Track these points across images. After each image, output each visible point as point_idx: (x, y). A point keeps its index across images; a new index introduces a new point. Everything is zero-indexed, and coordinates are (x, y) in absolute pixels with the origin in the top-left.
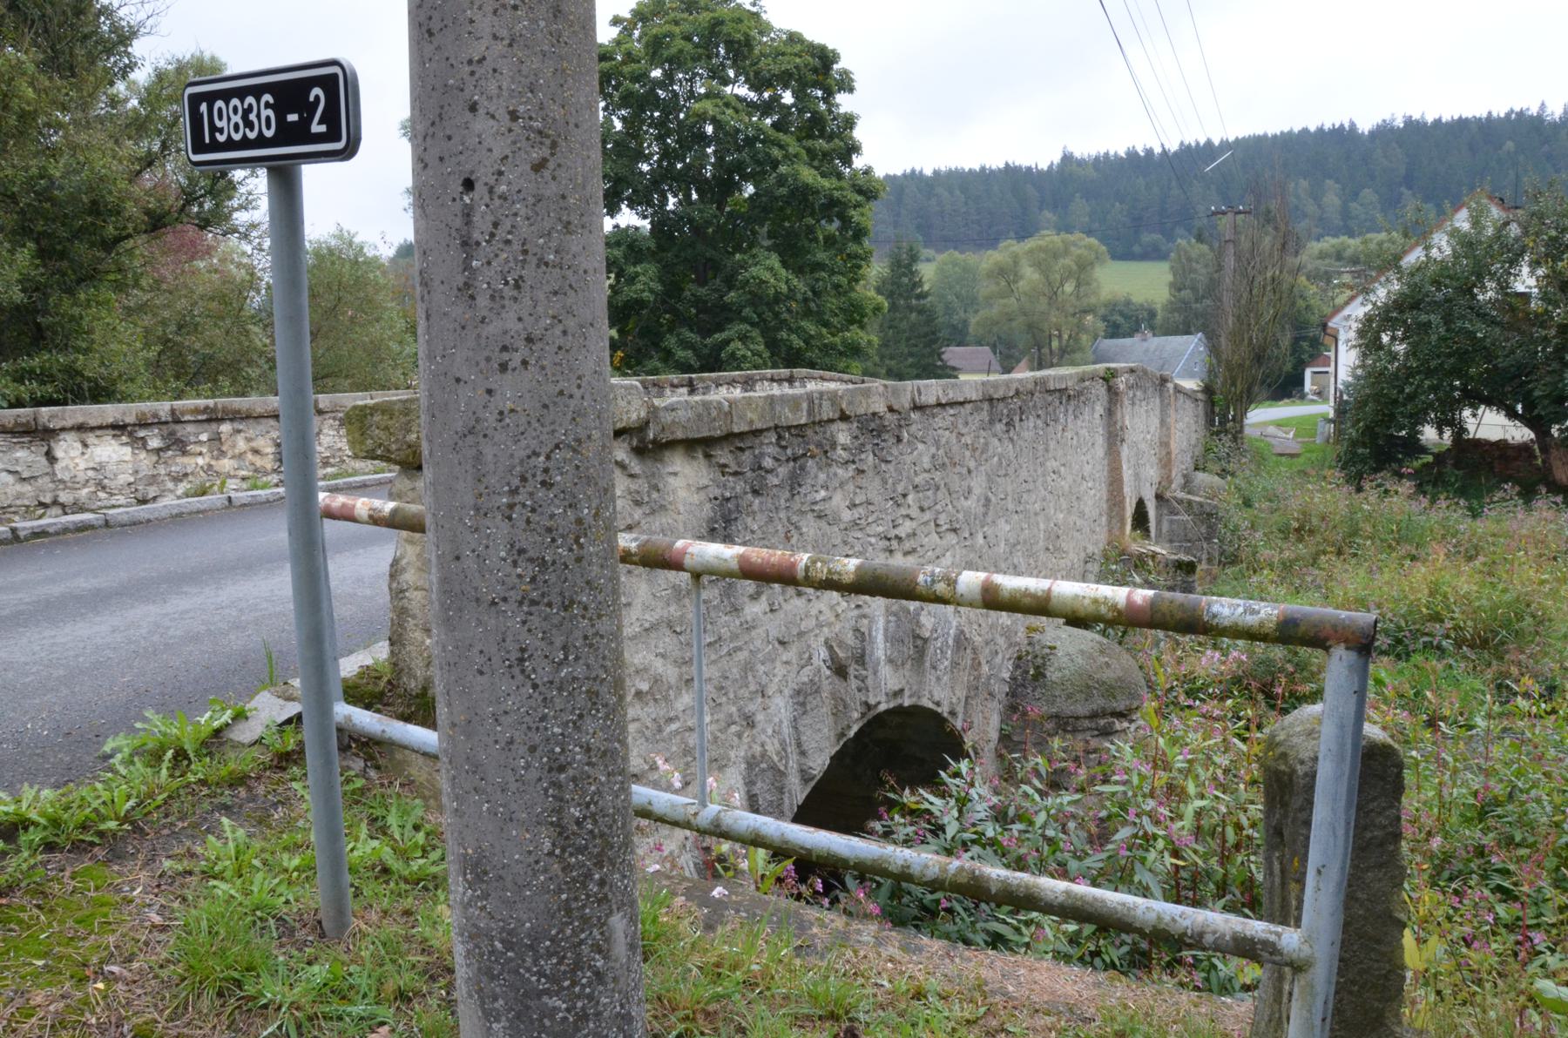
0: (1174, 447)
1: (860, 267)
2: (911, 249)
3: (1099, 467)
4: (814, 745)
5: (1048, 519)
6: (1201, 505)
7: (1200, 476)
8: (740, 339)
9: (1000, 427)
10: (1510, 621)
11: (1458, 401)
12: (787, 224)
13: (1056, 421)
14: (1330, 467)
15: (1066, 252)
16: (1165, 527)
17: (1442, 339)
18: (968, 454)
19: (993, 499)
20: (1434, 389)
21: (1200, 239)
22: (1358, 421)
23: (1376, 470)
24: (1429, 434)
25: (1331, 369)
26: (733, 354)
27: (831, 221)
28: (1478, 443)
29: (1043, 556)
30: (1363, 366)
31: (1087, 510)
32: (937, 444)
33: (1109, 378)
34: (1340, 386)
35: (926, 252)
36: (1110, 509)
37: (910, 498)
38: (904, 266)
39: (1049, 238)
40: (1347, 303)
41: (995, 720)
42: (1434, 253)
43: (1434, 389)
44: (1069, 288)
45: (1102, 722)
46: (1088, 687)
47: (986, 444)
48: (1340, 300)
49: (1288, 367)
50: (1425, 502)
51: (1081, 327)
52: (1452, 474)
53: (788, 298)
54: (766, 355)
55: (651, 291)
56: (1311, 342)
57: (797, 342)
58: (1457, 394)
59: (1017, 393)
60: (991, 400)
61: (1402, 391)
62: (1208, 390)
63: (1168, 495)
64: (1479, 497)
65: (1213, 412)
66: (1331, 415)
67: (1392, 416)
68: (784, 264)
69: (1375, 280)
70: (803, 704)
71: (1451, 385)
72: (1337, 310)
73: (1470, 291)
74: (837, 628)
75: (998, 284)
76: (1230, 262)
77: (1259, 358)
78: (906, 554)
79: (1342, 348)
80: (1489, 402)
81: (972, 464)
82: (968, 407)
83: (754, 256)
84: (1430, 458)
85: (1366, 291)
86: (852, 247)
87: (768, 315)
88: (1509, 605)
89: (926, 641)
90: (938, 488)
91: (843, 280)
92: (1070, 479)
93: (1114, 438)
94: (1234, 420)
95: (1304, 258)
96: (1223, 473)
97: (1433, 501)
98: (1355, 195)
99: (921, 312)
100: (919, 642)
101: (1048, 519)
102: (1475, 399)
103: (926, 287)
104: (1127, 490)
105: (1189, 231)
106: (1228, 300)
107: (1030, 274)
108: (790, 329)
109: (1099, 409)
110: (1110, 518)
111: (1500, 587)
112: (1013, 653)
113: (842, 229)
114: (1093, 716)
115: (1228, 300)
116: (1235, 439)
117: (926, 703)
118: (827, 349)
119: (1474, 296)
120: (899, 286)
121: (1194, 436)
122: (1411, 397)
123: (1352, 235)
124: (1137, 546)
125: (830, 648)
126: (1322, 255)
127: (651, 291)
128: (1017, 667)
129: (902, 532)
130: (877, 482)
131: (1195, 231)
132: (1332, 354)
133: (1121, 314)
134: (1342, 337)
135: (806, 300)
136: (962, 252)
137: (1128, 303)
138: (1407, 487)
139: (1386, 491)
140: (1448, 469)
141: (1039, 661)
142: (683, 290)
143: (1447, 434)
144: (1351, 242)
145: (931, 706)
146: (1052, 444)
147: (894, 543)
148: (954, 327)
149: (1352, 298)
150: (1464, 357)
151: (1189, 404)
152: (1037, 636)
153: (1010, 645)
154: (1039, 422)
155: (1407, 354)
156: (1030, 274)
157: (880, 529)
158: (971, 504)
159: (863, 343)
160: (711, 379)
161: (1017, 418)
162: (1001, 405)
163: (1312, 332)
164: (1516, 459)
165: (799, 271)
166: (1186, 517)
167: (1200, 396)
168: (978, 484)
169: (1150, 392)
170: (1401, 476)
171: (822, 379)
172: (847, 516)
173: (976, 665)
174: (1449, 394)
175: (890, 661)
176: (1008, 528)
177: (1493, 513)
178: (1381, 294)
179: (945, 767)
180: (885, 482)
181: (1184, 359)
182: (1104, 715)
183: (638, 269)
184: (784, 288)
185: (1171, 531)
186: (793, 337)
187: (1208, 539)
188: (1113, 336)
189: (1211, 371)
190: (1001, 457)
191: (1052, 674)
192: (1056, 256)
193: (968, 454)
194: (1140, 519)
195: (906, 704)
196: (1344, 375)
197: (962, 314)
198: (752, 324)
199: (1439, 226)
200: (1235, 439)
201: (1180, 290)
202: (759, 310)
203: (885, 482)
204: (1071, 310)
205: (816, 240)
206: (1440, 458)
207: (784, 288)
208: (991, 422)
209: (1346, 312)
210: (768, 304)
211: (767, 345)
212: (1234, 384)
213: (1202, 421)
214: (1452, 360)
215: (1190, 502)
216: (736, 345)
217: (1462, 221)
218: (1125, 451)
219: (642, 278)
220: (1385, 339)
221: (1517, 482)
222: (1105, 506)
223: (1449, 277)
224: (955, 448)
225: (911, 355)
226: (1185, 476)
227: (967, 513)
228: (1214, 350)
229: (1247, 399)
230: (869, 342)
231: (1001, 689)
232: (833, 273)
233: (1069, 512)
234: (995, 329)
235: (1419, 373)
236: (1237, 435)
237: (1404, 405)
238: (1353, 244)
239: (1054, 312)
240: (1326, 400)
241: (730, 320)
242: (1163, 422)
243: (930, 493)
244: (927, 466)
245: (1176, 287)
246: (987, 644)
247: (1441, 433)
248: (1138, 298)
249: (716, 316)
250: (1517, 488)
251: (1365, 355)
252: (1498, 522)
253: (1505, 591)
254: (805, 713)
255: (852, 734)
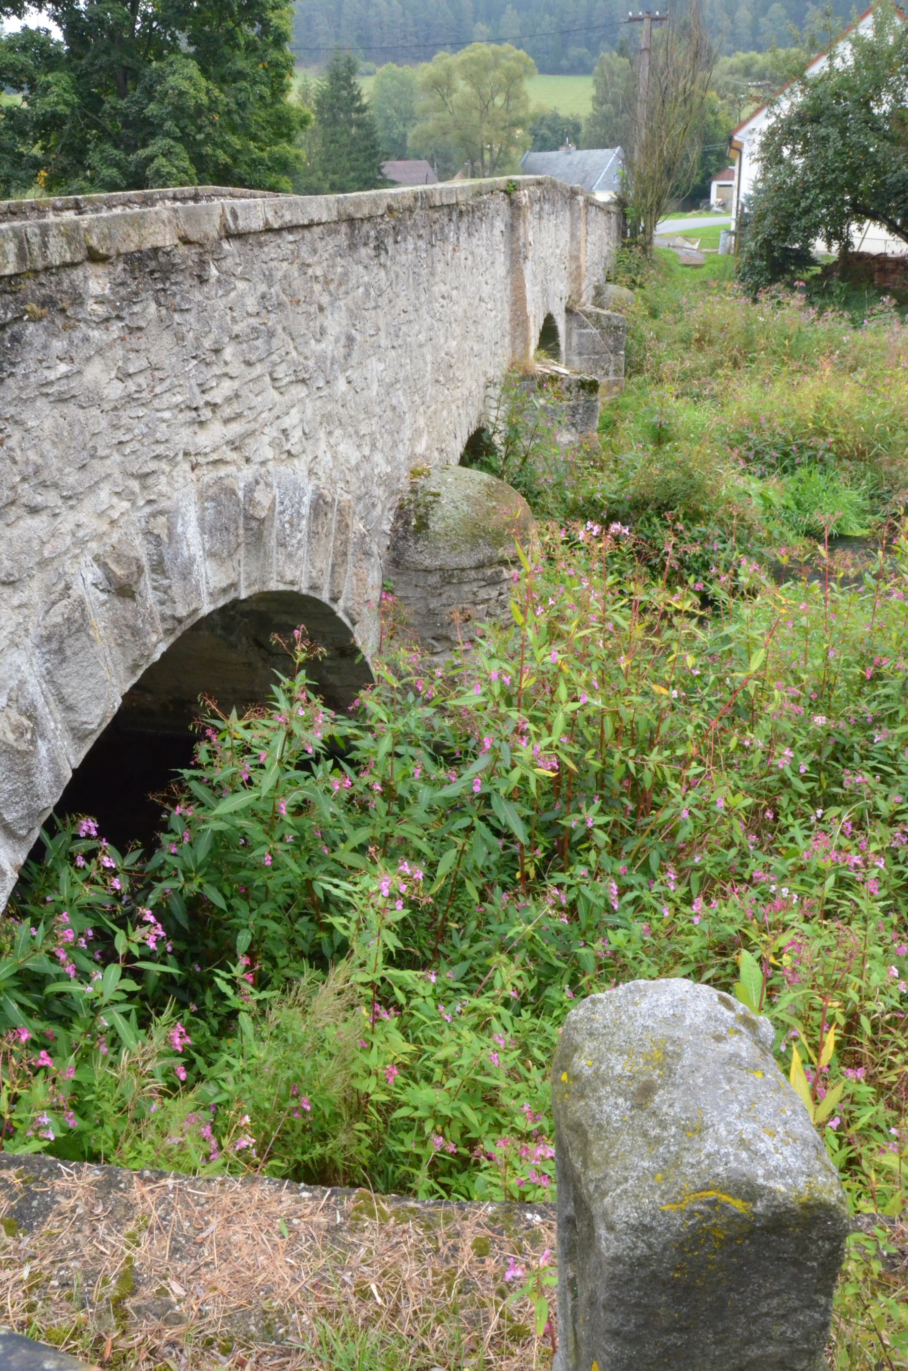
0: (585, 260)
1: (282, 76)
2: (349, 61)
3: (500, 287)
4: (85, 694)
5: (436, 349)
6: (609, 318)
7: (612, 288)
8: (164, 155)
9: (365, 252)
10: (884, 433)
11: (847, 216)
12: (207, 28)
13: (444, 239)
14: (730, 279)
15: (497, 65)
16: (575, 340)
17: (838, 153)
18: (317, 287)
19: (358, 337)
20: (827, 203)
21: (622, 52)
22: (758, 233)
23: (771, 282)
24: (819, 246)
25: (734, 183)
26: (158, 172)
27: (253, 26)
28: (862, 257)
29: (431, 390)
30: (764, 180)
31: (486, 334)
32: (269, 278)
33: (510, 191)
34: (742, 200)
35: (363, 66)
36: (514, 329)
37: (228, 353)
38: (342, 78)
39: (480, 49)
40: (753, 116)
41: (374, 577)
42: (838, 63)
43: (827, 203)
44: (499, 101)
45: (489, 572)
46: (474, 536)
47: (346, 274)
48: (745, 114)
49: (697, 180)
50: (812, 313)
51: (511, 141)
52: (837, 285)
53: (210, 110)
54: (193, 171)
55: (66, 103)
56: (718, 156)
57: (223, 157)
58: (846, 209)
59: (390, 209)
60: (351, 221)
61: (798, 205)
62: (621, 203)
63: (577, 309)
64: (861, 308)
65: (625, 223)
66: (733, 227)
67: (788, 229)
68: (204, 71)
69: (782, 92)
70: (61, 650)
71: (842, 200)
72: (742, 124)
73: (866, 104)
74: (115, 536)
75: (432, 97)
76: (644, 72)
77: (669, 172)
78: (227, 421)
79: (746, 161)
80: (874, 217)
81: (325, 300)
82: (317, 230)
83: (171, 64)
84: (818, 270)
85: (772, 103)
86: (273, 54)
87: (191, 129)
88: (885, 420)
89: (262, 521)
90: (271, 334)
91: (267, 92)
92: (464, 303)
93: (516, 256)
94: (644, 231)
95: (716, 73)
96: (633, 285)
97: (821, 313)
98: (765, 10)
99: (360, 125)
100: (254, 524)
101: (436, 349)
102: (862, 212)
103: (365, 100)
104: (531, 309)
105: (612, 44)
106: (641, 111)
107: (462, 87)
108: (215, 144)
109: (499, 225)
110: (514, 339)
111: (879, 401)
112: (394, 502)
113: (264, 32)
114: (480, 566)
115: (641, 111)
116: (644, 250)
117: (274, 585)
118: (255, 163)
119: (869, 110)
120: (338, 98)
121: (606, 248)
122: (807, 211)
123: (760, 49)
124: (543, 366)
125: (104, 566)
126: (733, 71)
127: (66, 103)
128: (398, 517)
129: (216, 396)
130: (167, 339)
131: (618, 45)
132: (736, 168)
133: (549, 128)
134: (746, 150)
135: (229, 112)
136: (400, 66)
137: (556, 117)
138: (798, 299)
139: (779, 303)
140: (834, 281)
141: (422, 510)
142: (103, 102)
143: (836, 246)
144: (759, 57)
145: (282, 587)
146: (440, 267)
147: (206, 413)
148: (394, 141)
149: (757, 111)
150: (855, 172)
151: (601, 218)
152: (421, 481)
153: (392, 493)
154: (421, 244)
155: (804, 170)
156: (462, 87)
157: (179, 398)
158: (329, 347)
159: (291, 158)
160: (100, 200)
161: (389, 241)
162: (366, 226)
163: (719, 146)
164: (893, 272)
165: (222, 80)
166: (594, 331)
167: (613, 208)
168: (335, 323)
169: (559, 205)
170: (793, 289)
171: (232, 196)
172: (115, 391)
173: (343, 527)
174: (839, 209)
175: (211, 554)
176: (382, 366)
177: (873, 326)
178: (785, 106)
179: (278, 682)
180: (180, 338)
181: (601, 172)
182: (491, 565)
183: (50, 78)
184: (205, 100)
185: (580, 344)
186: (220, 153)
187: (615, 351)
188: (541, 149)
189: (624, 184)
190: (367, 286)
191: (436, 525)
192: (486, 69)
193: (317, 287)
194: (549, 333)
195: (243, 595)
196: (747, 189)
197: (401, 128)
198: (175, 139)
199: (843, 36)
200: (644, 250)
201: (602, 104)
202: (182, 124)
203: (180, 338)
204: (502, 124)
205: (238, 46)
206: (828, 270)
207: (205, 100)
208: (353, 247)
209: (750, 126)
210: (191, 117)
211: (192, 160)
212: (644, 196)
213: (614, 233)
214: (846, 175)
215: (598, 315)
216: (161, 161)
217: (866, 29)
218: (529, 269)
219: (54, 89)
220: (786, 152)
221: (894, 295)
222: (508, 327)
223: (850, 89)
224: (298, 283)
225: (353, 169)
226: (596, 288)
227: (321, 359)
228: (628, 162)
229: (657, 211)
230: (297, 157)
231: (378, 547)
232: (254, 83)
233: (464, 338)
234: (431, 143)
235: (814, 187)
236: (646, 247)
237: (799, 219)
238: (762, 59)
239: (486, 126)
240: (729, 212)
241: (153, 135)
242: (573, 236)
243: (259, 343)
244: (252, 309)
245: (598, 101)
246: (359, 499)
247: (830, 245)
248: (564, 113)
249: (144, 129)
250: (894, 301)
251: (766, 169)
252: (876, 333)
253: (883, 406)
254: (63, 661)
255: (157, 656)
